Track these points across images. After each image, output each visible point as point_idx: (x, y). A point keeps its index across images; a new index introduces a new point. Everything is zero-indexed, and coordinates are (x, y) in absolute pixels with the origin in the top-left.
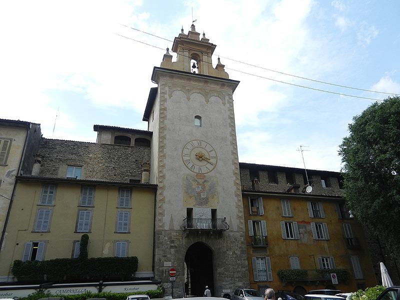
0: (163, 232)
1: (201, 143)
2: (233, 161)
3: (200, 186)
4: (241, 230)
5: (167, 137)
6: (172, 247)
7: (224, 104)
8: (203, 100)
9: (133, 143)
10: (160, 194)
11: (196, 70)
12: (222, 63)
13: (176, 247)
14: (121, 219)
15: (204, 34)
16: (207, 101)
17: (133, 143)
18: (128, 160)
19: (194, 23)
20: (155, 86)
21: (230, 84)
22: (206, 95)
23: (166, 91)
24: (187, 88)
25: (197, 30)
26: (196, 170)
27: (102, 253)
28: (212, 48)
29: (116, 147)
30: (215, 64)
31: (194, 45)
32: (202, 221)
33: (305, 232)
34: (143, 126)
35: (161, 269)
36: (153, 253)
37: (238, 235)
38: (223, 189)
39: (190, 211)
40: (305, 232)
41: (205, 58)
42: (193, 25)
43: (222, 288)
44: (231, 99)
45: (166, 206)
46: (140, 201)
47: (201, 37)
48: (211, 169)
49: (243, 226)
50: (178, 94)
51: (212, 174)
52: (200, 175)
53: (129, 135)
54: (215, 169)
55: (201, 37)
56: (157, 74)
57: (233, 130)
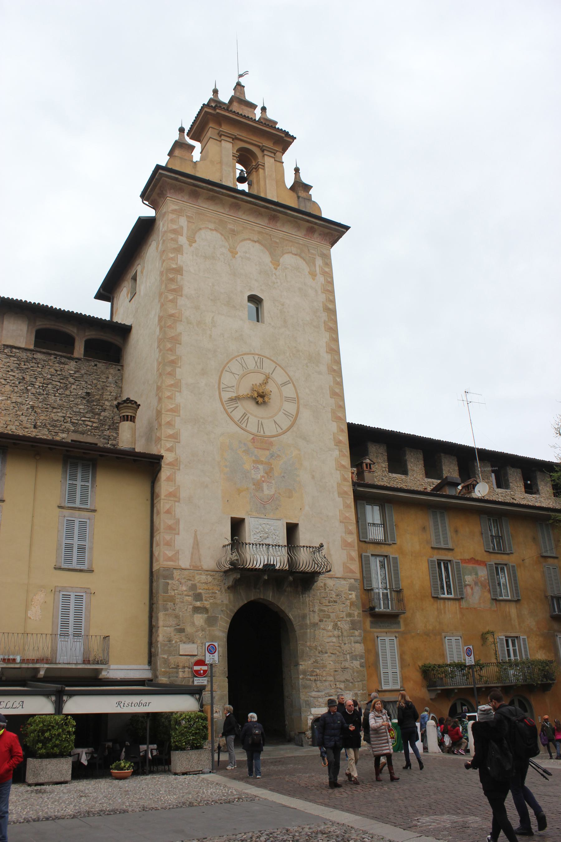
0: (176, 574)
1: (262, 362)
2: (333, 412)
3: (261, 467)
4: (350, 575)
5: (185, 338)
6: (196, 610)
7: (313, 275)
8: (267, 259)
9: (79, 350)
10: (169, 479)
11: (244, 187)
12: (305, 179)
13: (204, 610)
14: (70, 536)
15: (264, 109)
16: (276, 264)
17: (79, 350)
18: (68, 392)
19: (242, 80)
20: (150, 212)
21: (327, 231)
22: (273, 249)
23: (182, 227)
24: (230, 226)
25: (249, 97)
26: (252, 427)
27: (26, 618)
28: (284, 140)
29: (39, 356)
30: (289, 181)
31: (238, 127)
32: (264, 550)
33: (476, 584)
34: (102, 310)
35: (172, 659)
36: (151, 617)
37: (344, 586)
38: (313, 477)
39: (237, 525)
40: (476, 584)
41: (268, 161)
42: (238, 84)
43: (309, 705)
44: (328, 263)
45: (182, 510)
46: (114, 499)
47: (258, 114)
48: (285, 428)
49: (355, 567)
50: (209, 238)
51: (287, 438)
52: (261, 442)
53: (71, 330)
54: (295, 428)
55: (258, 114)
56: (157, 188)
57: (329, 282)
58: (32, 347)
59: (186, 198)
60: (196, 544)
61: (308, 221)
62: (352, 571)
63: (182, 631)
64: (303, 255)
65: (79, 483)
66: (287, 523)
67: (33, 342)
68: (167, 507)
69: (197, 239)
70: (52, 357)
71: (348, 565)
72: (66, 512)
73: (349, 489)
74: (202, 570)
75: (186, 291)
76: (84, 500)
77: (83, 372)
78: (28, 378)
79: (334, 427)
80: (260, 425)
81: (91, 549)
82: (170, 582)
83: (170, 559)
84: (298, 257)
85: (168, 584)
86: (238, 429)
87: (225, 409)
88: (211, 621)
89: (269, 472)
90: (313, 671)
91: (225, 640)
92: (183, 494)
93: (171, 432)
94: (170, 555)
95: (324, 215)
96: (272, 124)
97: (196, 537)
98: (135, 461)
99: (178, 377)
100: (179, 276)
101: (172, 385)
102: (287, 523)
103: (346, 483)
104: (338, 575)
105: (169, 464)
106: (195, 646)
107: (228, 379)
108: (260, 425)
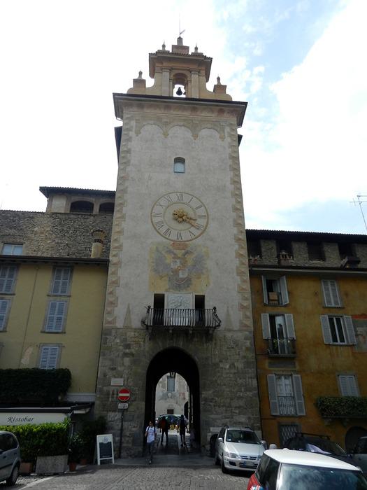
0: (113, 331)
3: (178, 261)
5: (130, 189)
6: (126, 355)
7: (222, 138)
8: (189, 134)
9: (96, 209)
10: (113, 273)
16: (195, 136)
17: (96, 209)
25: (185, 44)
26: (173, 236)
29: (72, 216)
43: (209, 424)
45: (120, 292)
49: (250, 323)
53: (92, 200)
58: (68, 212)
59: (135, 109)
60: (129, 312)
61: (217, 106)
62: (246, 326)
63: (113, 369)
64: (216, 128)
65: (61, 281)
66: (196, 296)
67: (69, 209)
68: (111, 290)
69: (142, 131)
70: (80, 216)
71: (244, 322)
72: (51, 298)
73: (246, 270)
74: (131, 329)
75: (132, 162)
76: (63, 291)
77: (97, 222)
78: (65, 229)
79: (235, 231)
80: (179, 235)
81: (65, 319)
82: (108, 337)
83: (109, 323)
84: (212, 130)
85: (107, 338)
86: (164, 240)
87: (155, 228)
88: (134, 362)
89: (184, 264)
90: (213, 399)
91: (145, 375)
92: (122, 282)
93: (117, 245)
94: (110, 320)
95: (233, 100)
96: (201, 55)
97: (129, 307)
98: (98, 264)
99: (124, 212)
100: (129, 155)
101: (119, 218)
102: (196, 296)
103: (244, 266)
104: (235, 329)
105: (114, 264)
106: (122, 379)
107: (157, 209)
108: (179, 235)
